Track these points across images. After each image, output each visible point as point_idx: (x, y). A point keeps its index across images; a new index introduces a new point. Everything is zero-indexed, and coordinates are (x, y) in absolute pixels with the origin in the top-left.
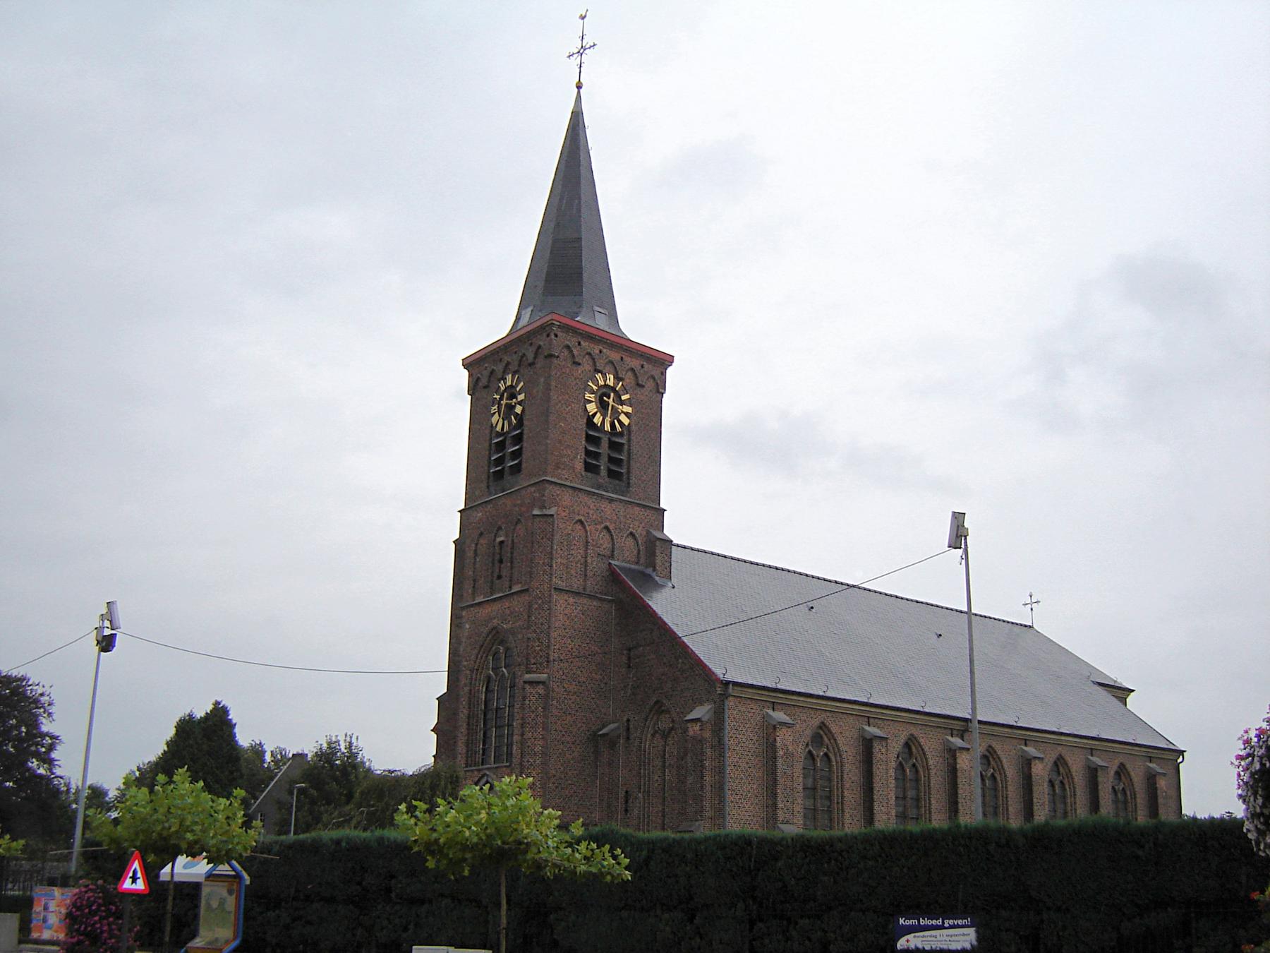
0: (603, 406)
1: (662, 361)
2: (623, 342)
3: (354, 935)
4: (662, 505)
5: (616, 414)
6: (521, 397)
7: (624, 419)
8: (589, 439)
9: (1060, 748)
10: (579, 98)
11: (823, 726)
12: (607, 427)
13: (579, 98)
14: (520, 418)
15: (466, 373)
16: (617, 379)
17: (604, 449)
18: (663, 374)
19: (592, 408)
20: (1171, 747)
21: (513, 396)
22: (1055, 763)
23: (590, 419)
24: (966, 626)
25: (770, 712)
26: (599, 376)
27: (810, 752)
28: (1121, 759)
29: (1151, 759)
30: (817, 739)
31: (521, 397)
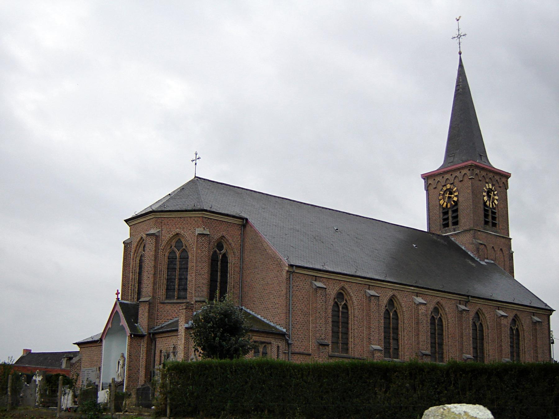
0: (489, 196)
1: (507, 176)
2: (493, 169)
3: (157, 370)
4: (510, 237)
5: (494, 199)
6: (456, 194)
7: (496, 201)
8: (485, 210)
9: (342, 284)
10: (461, 66)
11: (343, 288)
12: (491, 206)
13: (461, 66)
14: (456, 203)
15: (423, 181)
16: (493, 185)
17: (490, 213)
18: (507, 181)
19: (486, 198)
20: (547, 308)
21: (451, 193)
22: (477, 313)
23: (485, 203)
24: (226, 212)
25: (415, 298)
26: (487, 185)
27: (433, 317)
28: (438, 299)
29: (316, 278)
30: (436, 310)
31: (456, 194)
